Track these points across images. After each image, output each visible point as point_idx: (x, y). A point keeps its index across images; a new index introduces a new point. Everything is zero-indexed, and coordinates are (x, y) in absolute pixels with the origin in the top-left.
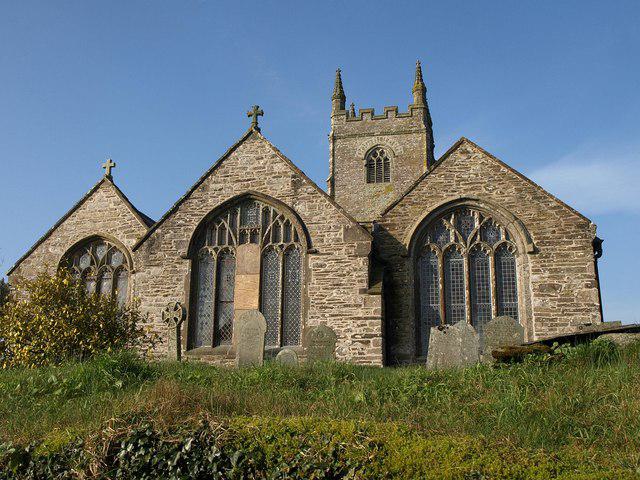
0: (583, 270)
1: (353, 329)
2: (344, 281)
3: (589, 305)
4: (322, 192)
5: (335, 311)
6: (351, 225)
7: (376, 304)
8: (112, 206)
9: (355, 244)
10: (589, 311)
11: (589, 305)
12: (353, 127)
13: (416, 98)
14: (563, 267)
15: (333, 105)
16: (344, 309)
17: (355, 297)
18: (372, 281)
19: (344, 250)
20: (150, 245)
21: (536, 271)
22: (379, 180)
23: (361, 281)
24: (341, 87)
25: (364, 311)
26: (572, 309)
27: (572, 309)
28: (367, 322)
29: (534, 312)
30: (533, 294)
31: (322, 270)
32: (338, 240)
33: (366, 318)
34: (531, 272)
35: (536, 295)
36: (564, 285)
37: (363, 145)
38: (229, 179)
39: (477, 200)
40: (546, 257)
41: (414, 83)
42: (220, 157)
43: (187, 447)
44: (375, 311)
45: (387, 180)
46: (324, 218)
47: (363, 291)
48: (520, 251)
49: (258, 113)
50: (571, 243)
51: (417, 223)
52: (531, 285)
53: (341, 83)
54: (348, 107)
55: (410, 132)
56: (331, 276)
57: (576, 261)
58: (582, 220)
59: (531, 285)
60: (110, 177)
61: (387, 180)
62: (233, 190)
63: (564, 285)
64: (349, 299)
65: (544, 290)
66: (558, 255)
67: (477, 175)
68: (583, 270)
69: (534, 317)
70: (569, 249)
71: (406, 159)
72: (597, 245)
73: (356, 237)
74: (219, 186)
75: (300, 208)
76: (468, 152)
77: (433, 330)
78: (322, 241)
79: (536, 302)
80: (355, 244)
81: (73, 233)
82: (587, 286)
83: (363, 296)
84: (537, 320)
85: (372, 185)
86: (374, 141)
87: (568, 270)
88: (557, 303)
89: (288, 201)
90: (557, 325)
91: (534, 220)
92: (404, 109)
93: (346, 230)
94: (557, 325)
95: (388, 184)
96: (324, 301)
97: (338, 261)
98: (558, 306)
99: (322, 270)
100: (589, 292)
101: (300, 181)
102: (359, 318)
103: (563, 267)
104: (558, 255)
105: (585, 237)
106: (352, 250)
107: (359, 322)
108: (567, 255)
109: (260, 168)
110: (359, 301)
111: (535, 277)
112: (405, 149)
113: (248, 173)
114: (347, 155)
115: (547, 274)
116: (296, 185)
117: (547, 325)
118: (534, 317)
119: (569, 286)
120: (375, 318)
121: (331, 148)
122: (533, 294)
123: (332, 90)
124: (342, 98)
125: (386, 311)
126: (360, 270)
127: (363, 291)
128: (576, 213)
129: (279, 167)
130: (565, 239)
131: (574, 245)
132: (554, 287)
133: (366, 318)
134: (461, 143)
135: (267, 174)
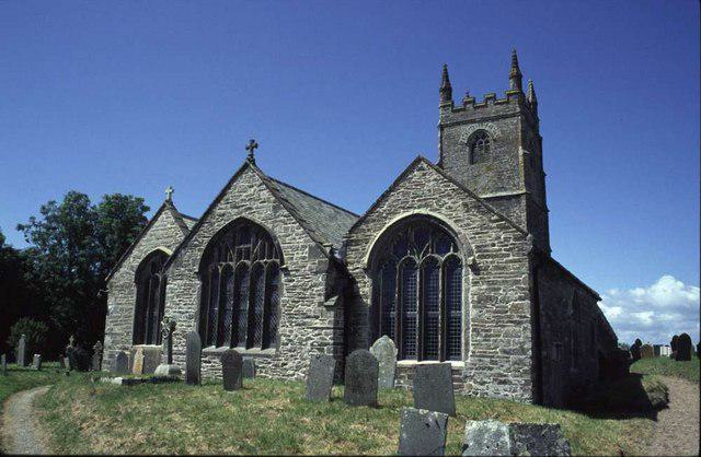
0: (517, 282)
12: (459, 117)
17: (312, 309)
21: (475, 283)
23: (319, 295)
24: (448, 80)
32: (304, 258)
33: (323, 328)
35: (474, 307)
47: (320, 304)
49: (253, 146)
50: (508, 255)
52: (470, 296)
53: (447, 76)
59: (470, 296)
60: (169, 202)
65: (481, 301)
66: (497, 268)
68: (517, 282)
73: (316, 256)
74: (222, 211)
77: (599, 303)
79: (473, 313)
86: (477, 127)
90: (490, 336)
92: (501, 98)
93: (311, 248)
94: (490, 336)
102: (316, 329)
104: (497, 268)
107: (317, 332)
111: (473, 289)
114: (453, 140)
120: (328, 328)
122: (471, 305)
123: (439, 84)
124: (447, 91)
129: (265, 194)
131: (511, 258)
132: (489, 299)
134: (419, 160)
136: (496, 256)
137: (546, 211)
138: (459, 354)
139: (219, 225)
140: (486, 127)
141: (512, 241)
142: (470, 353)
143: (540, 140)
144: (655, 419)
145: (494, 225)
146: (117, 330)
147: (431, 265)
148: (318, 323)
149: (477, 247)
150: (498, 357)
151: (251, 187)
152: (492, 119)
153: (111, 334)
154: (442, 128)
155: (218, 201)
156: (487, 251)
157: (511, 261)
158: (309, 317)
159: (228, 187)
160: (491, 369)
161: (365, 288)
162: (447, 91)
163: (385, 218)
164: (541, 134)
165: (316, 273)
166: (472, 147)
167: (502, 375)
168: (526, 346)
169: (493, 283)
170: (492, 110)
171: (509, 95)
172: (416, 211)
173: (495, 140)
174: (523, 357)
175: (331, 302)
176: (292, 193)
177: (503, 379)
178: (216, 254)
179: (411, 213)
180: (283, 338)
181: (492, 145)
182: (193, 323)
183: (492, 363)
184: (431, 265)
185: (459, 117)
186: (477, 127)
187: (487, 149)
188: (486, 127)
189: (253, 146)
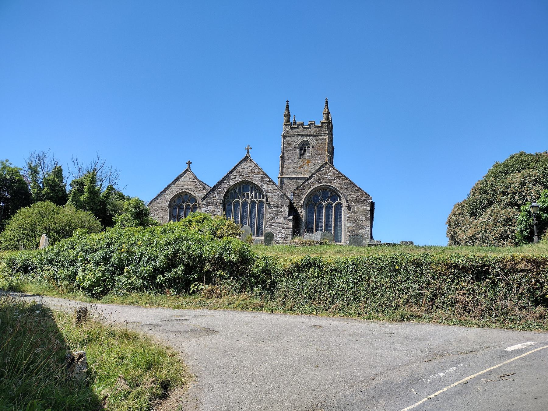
4: (274, 183)
7: (291, 224)
12: (293, 132)
13: (323, 118)
15: (284, 120)
17: (283, 221)
18: (289, 215)
24: (288, 110)
33: (286, 228)
37: (297, 141)
41: (323, 109)
42: (235, 165)
43: (329, 194)
45: (308, 157)
47: (286, 218)
48: (344, 205)
49: (249, 149)
51: (307, 193)
53: (288, 108)
54: (292, 120)
62: (240, 179)
71: (319, 148)
72: (372, 205)
81: (176, 189)
86: (304, 139)
92: (319, 124)
95: (308, 159)
107: (284, 230)
116: (262, 178)
121: (283, 140)
123: (284, 112)
124: (288, 116)
125: (294, 226)
127: (286, 218)
138: (341, 240)
139: (232, 183)
140: (309, 139)
141: (363, 198)
145: (357, 191)
147: (245, 203)
152: (313, 136)
154: (284, 137)
155: (232, 171)
159: (238, 165)
161: (303, 214)
162: (288, 116)
163: (311, 185)
166: (301, 150)
170: (313, 130)
171: (323, 123)
172: (324, 184)
173: (313, 147)
175: (291, 217)
179: (322, 184)
181: (311, 149)
184: (245, 203)
185: (293, 132)
186: (304, 139)
187: (309, 151)
188: (309, 139)
189: (249, 149)
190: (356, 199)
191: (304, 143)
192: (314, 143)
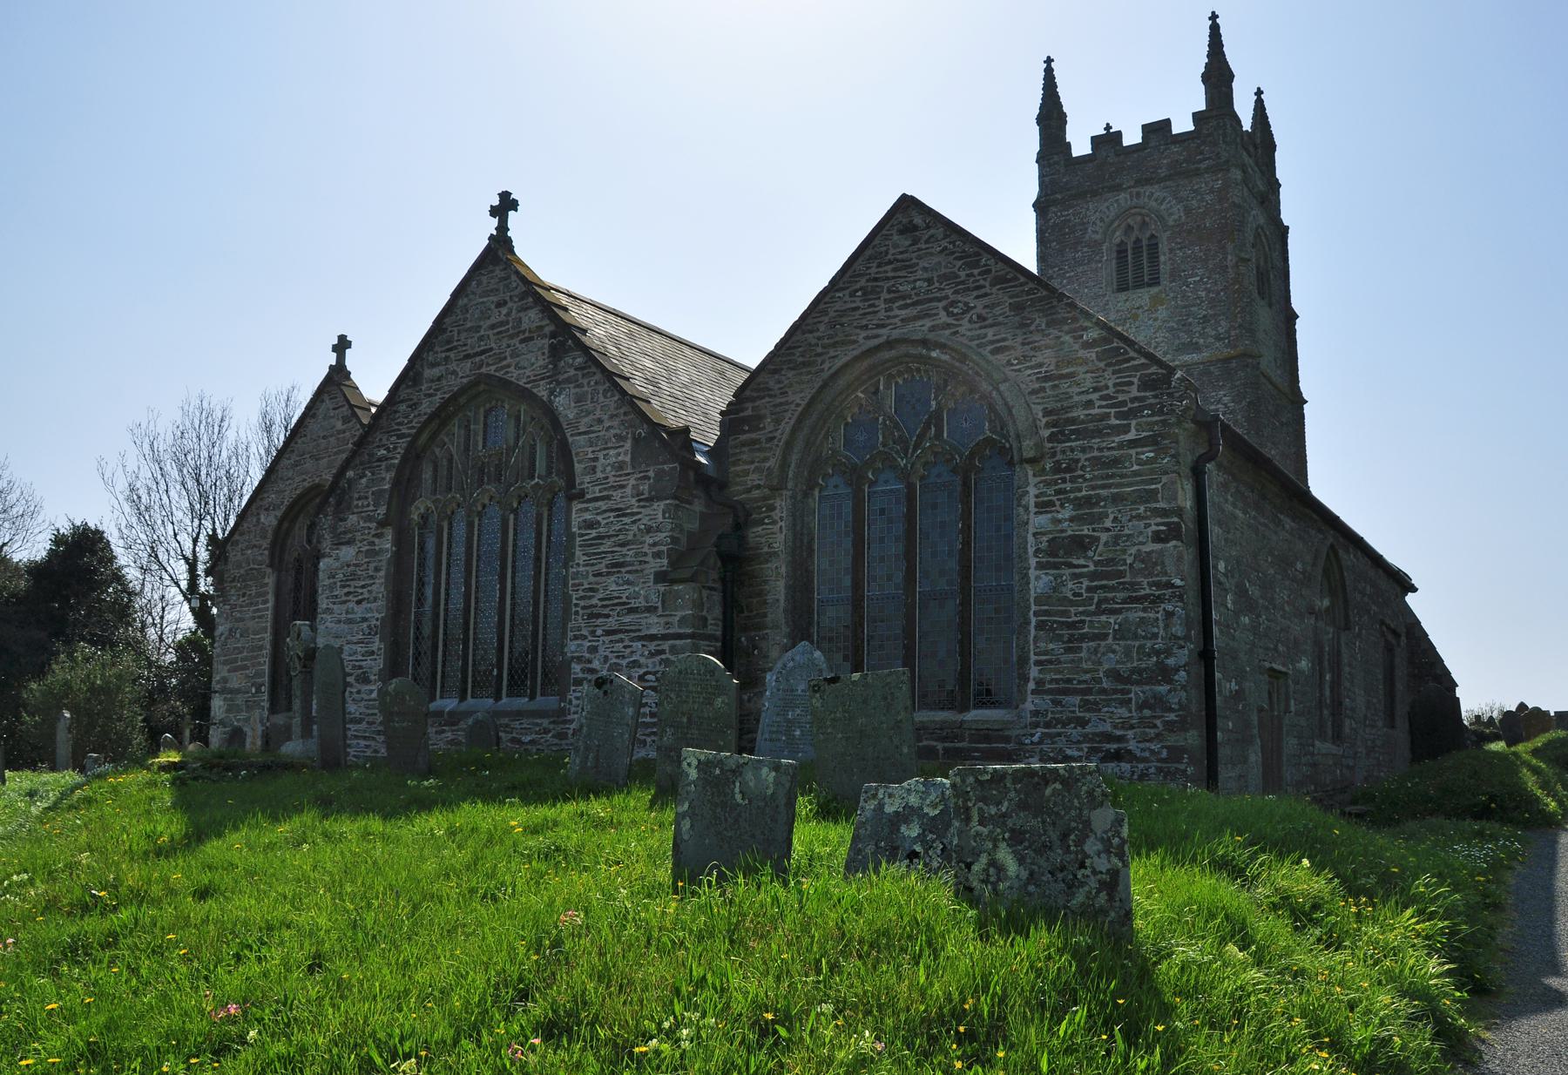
1: (642, 660)
2: (629, 554)
3: (1158, 585)
5: (612, 623)
6: (642, 431)
8: (339, 425)
9: (651, 474)
10: (1158, 600)
11: (1158, 585)
14: (1103, 492)
16: (627, 619)
17: (647, 591)
19: (628, 490)
20: (339, 503)
21: (1044, 506)
22: (1139, 284)
23: (657, 555)
25: (662, 620)
26: (1120, 595)
27: (1120, 595)
28: (666, 645)
29: (1033, 608)
30: (1033, 562)
31: (594, 533)
33: (665, 637)
34: (1032, 509)
35: (1040, 566)
36: (1104, 537)
38: (452, 355)
39: (924, 343)
40: (1069, 470)
44: (682, 621)
46: (600, 421)
47: (661, 577)
55: (1197, 173)
56: (607, 546)
57: (1136, 474)
58: (1154, 369)
59: (1030, 538)
61: (1155, 281)
63: (1104, 537)
64: (636, 596)
66: (1096, 462)
67: (930, 281)
69: (1033, 620)
70: (1121, 446)
75: (564, 403)
76: (916, 228)
77: (1410, 599)
78: (594, 469)
80: (651, 474)
82: (1158, 538)
83: (661, 588)
84: (1041, 626)
85: (1122, 296)
87: (1116, 499)
88: (1086, 583)
89: (542, 392)
90: (1083, 638)
91: (1047, 379)
93: (637, 440)
94: (1083, 638)
95: (1154, 290)
96: (594, 601)
97: (620, 512)
98: (1089, 589)
99: (594, 533)
100: (1161, 553)
101: (563, 344)
102: (652, 638)
103: (1103, 492)
105: (1161, 412)
106: (645, 487)
107: (652, 646)
108: (1116, 462)
109: (502, 324)
110: (655, 600)
111: (1039, 521)
112: (1188, 211)
113: (481, 339)
115: (1067, 513)
117: (1059, 638)
118: (1033, 620)
119: (1116, 540)
126: (658, 530)
127: (661, 577)
128: (1142, 352)
130: (1114, 422)
131: (1132, 435)
132: (1081, 545)
133: (665, 637)
135: (511, 337)
136: (1098, 433)
137: (1297, 402)
141: (1134, 392)
142: (1031, 686)
143: (1284, 231)
144: (1108, 127)
146: (236, 681)
148: (654, 624)
149: (1047, 413)
150: (1103, 691)
151: (499, 305)
153: (223, 691)
156: (1073, 421)
157: (1133, 443)
158: (632, 611)
160: (1083, 723)
164: (1286, 217)
165: (650, 499)
167: (1109, 737)
168: (1171, 661)
169: (1089, 501)
174: (1163, 689)
176: (559, 296)
177: (1113, 746)
178: (427, 474)
180: (576, 668)
182: (377, 644)
183: (1085, 705)
190: (1089, 404)
191: (1132, 223)
192: (1171, 214)
